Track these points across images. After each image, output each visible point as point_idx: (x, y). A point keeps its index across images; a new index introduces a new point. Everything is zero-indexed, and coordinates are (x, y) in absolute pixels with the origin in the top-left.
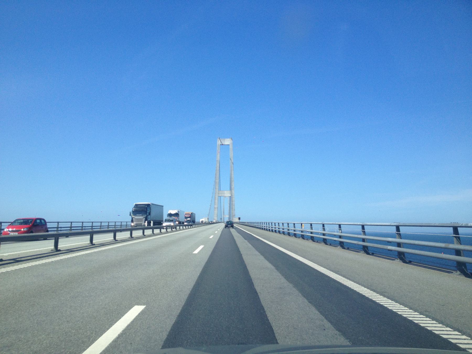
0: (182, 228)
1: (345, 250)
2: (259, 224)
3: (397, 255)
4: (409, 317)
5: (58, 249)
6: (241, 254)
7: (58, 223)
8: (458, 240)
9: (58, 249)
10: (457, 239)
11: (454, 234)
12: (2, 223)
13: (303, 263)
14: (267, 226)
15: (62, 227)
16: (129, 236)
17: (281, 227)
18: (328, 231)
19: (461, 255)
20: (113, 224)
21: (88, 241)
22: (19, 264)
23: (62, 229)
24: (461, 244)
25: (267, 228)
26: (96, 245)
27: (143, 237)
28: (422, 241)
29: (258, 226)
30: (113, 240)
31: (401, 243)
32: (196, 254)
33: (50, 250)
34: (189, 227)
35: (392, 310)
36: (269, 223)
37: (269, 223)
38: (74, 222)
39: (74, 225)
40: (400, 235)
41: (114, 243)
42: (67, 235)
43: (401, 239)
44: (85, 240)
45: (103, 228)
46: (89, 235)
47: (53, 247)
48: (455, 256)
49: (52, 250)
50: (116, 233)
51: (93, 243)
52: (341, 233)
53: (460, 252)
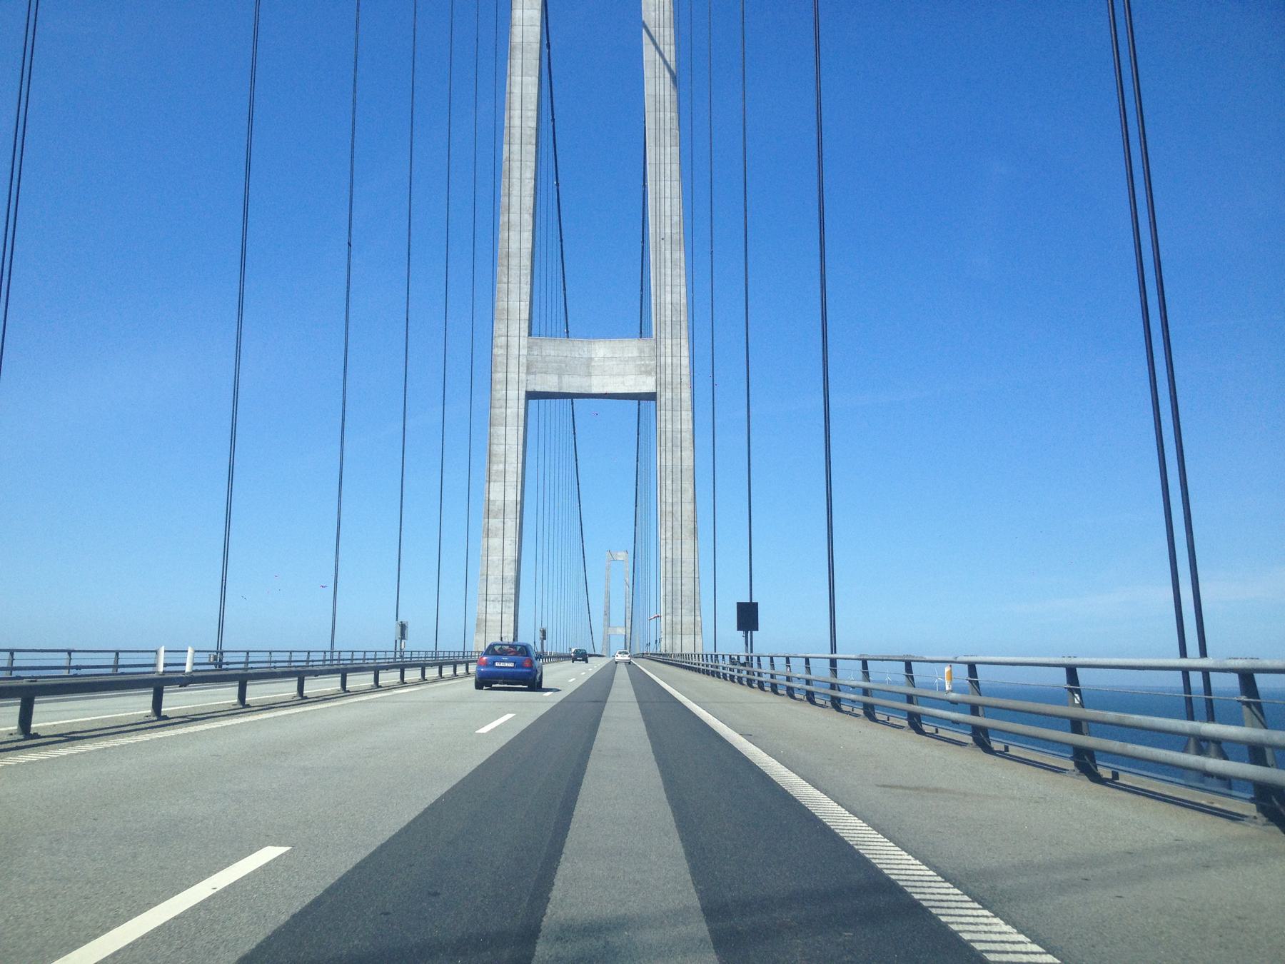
1: (875, 724)
2: (703, 660)
7: (12, 654)
8: (1253, 712)
11: (1242, 694)
15: (231, 661)
17: (765, 671)
23: (231, 666)
25: (741, 675)
27: (343, 695)
29: (703, 665)
35: (921, 904)
36: (707, 655)
37: (723, 657)
39: (253, 657)
42: (316, 673)
43: (1265, 730)
45: (313, 666)
50: (346, 676)
51: (304, 695)
52: (1082, 705)
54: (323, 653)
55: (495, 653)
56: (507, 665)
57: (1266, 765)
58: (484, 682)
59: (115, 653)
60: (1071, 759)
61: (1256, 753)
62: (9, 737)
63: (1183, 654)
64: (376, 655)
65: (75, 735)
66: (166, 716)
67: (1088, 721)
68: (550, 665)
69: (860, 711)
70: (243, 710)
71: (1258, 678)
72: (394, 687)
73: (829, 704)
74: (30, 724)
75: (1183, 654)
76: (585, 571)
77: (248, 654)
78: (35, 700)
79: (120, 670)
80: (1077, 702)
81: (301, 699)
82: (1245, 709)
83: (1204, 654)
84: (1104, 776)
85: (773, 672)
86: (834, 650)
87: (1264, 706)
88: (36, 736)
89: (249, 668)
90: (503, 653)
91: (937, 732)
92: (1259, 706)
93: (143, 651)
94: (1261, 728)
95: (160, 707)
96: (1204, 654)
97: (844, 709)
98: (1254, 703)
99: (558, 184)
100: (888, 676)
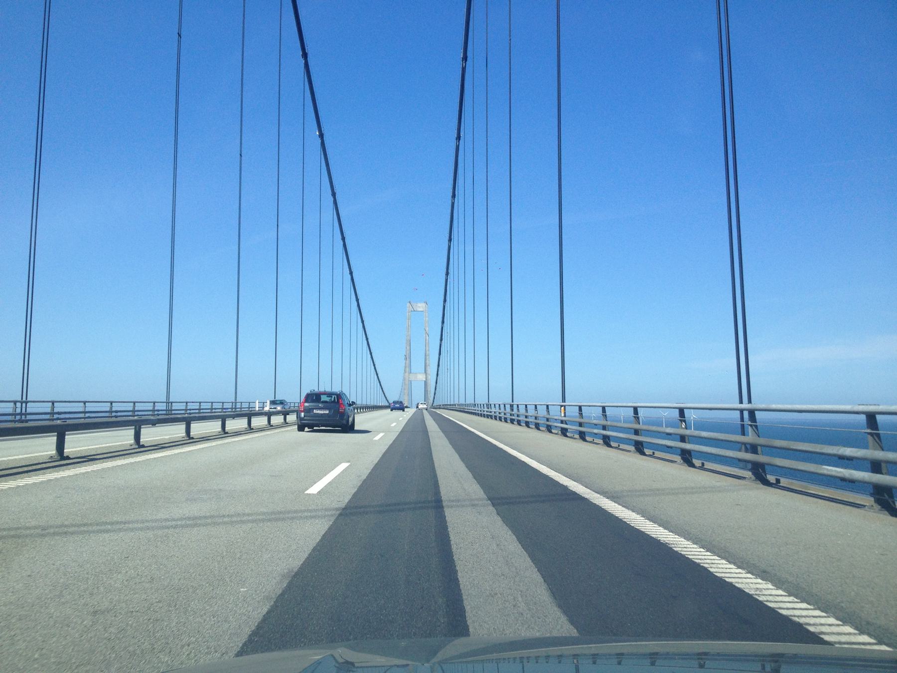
2: (481, 408)
4: (697, 559)
5: (65, 455)
7: (111, 404)
8: (875, 440)
13: (528, 465)
14: (500, 411)
17: (531, 414)
18: (644, 423)
19: (881, 470)
20: (209, 406)
22: (108, 461)
24: (883, 450)
25: (500, 415)
26: (147, 447)
29: (478, 411)
30: (220, 432)
32: (392, 427)
36: (480, 405)
37: (495, 406)
38: (89, 402)
39: (139, 407)
41: (131, 454)
42: (154, 423)
44: (45, 446)
46: (53, 436)
47: (53, 452)
49: (52, 457)
50: (251, 418)
51: (141, 444)
52: (686, 428)
53: (685, 438)
54: (12, 404)
57: (881, 473)
59: (153, 404)
61: (876, 467)
63: (741, 402)
64: (187, 406)
65: (91, 457)
68: (366, 414)
69: (577, 436)
70: (224, 436)
71: (878, 417)
73: (560, 432)
74: (140, 440)
75: (741, 402)
78: (66, 433)
79: (202, 411)
80: (683, 426)
81: (139, 448)
82: (870, 438)
83: (750, 401)
85: (518, 413)
86: (564, 400)
87: (758, 427)
88: (68, 458)
92: (756, 426)
93: (104, 402)
95: (139, 442)
96: (750, 401)
97: (613, 446)
98: (754, 425)
100: (593, 414)
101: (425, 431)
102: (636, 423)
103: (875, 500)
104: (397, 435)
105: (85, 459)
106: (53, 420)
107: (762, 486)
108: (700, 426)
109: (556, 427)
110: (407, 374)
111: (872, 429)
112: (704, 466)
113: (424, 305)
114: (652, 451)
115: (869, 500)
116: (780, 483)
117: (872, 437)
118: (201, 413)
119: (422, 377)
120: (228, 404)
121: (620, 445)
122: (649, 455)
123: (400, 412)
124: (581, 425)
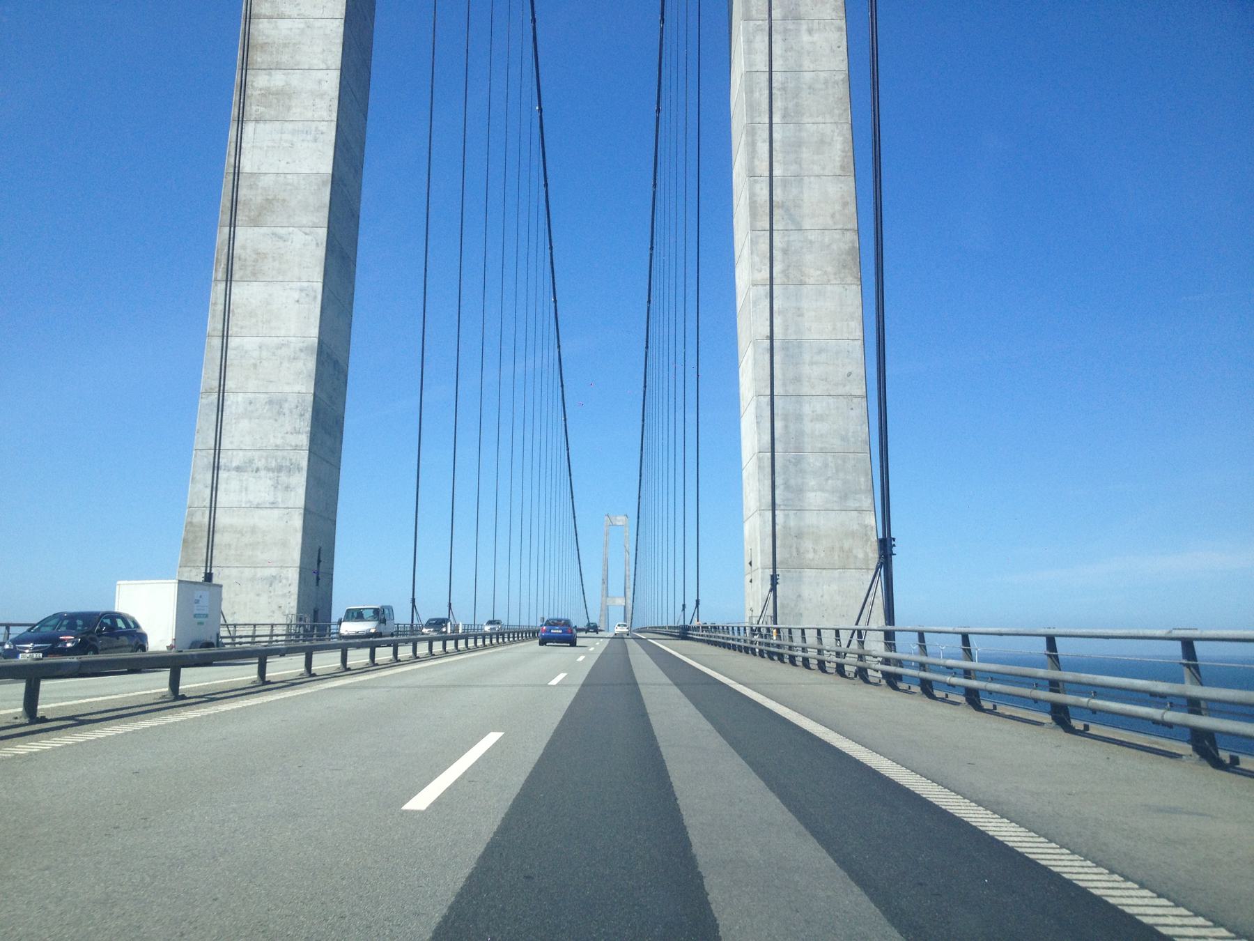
0: (464, 646)
2: (739, 633)
3: (1189, 740)
4: (1030, 853)
5: (267, 680)
6: (685, 827)
9: (267, 680)
10: (1191, 671)
12: (11, 627)
16: (411, 654)
18: (981, 660)
21: (16, 707)
26: (190, 698)
28: (1110, 675)
31: (1060, 681)
33: (299, 674)
34: (450, 645)
36: (733, 628)
37: (745, 629)
40: (1058, 660)
43: (1060, 672)
44: (246, 673)
47: (302, 670)
48: (1188, 715)
50: (312, 654)
55: (550, 625)
56: (557, 631)
58: (542, 643)
60: (964, 695)
62: (14, 721)
65: (213, 696)
66: (44, 717)
67: (929, 664)
69: (917, 689)
72: (332, 676)
74: (178, 686)
76: (583, 585)
77: (272, 627)
81: (30, 723)
82: (1186, 670)
84: (1076, 728)
85: (804, 645)
89: (273, 641)
90: (556, 625)
91: (947, 696)
92: (1196, 667)
94: (1197, 685)
98: (1193, 665)
99: (555, 301)
100: (944, 650)
101: (632, 687)
102: (921, 655)
103: (1193, 748)
104: (573, 696)
105: (204, 699)
106: (254, 643)
107: (840, 677)
108: (1079, 666)
109: (990, 692)
110: (604, 598)
111: (1189, 660)
112: (996, 709)
113: (624, 518)
114: (1083, 723)
115: (1185, 748)
116: (1238, 763)
117: (1188, 669)
118: (257, 642)
119: (621, 602)
120: (247, 628)
121: (1091, 725)
122: (988, 710)
123: (567, 650)
124: (924, 667)
